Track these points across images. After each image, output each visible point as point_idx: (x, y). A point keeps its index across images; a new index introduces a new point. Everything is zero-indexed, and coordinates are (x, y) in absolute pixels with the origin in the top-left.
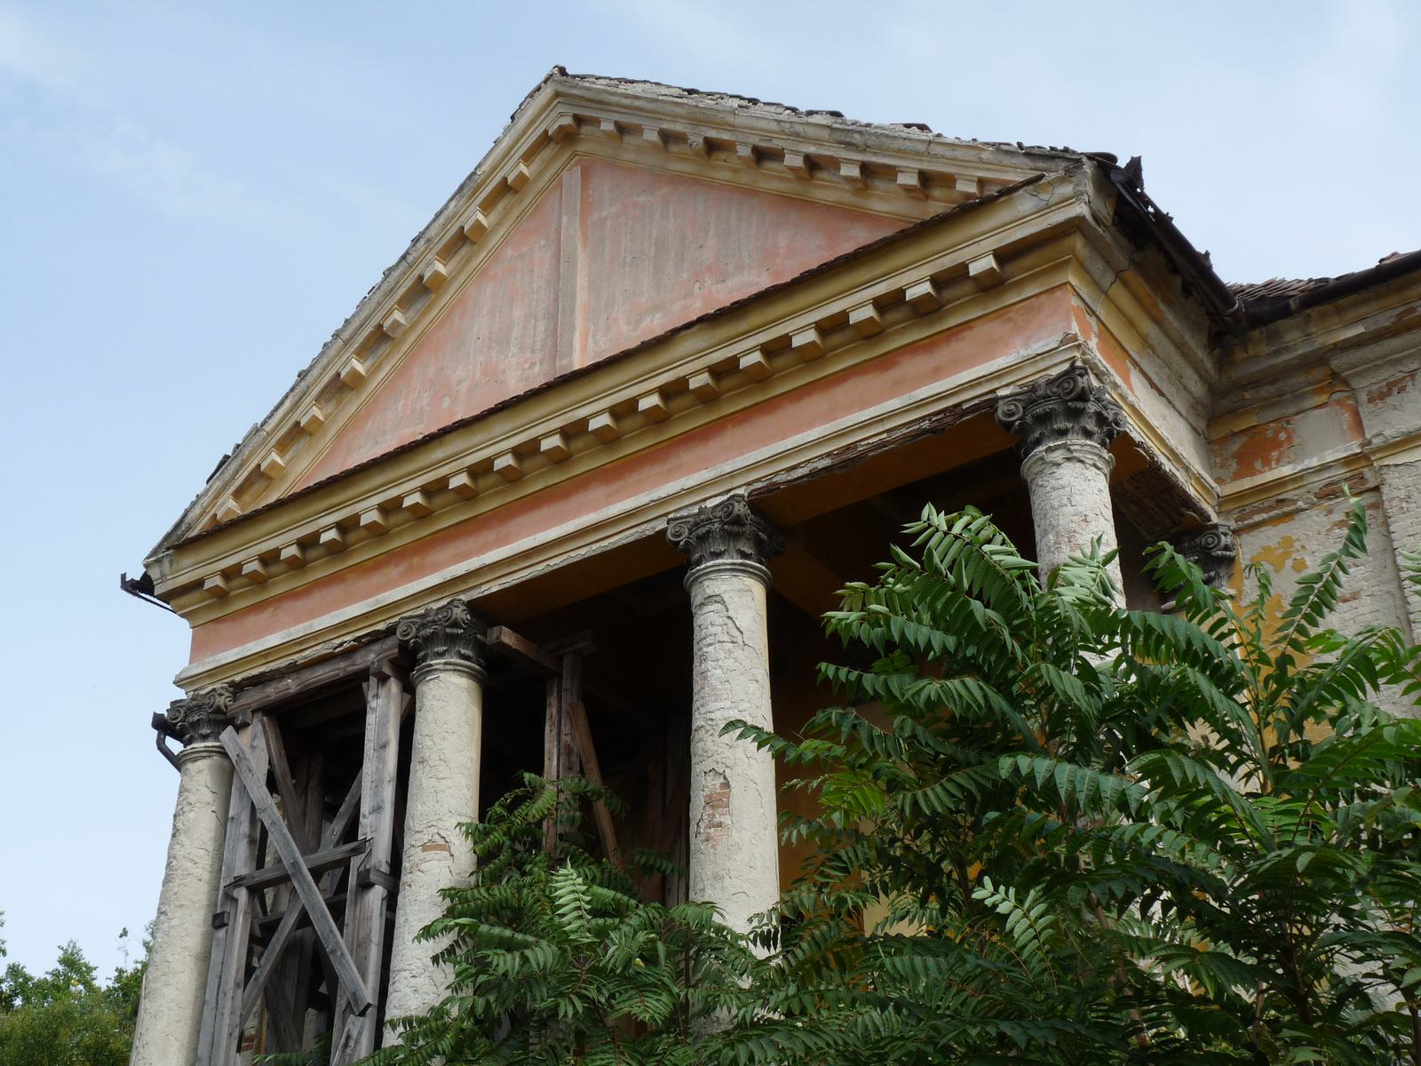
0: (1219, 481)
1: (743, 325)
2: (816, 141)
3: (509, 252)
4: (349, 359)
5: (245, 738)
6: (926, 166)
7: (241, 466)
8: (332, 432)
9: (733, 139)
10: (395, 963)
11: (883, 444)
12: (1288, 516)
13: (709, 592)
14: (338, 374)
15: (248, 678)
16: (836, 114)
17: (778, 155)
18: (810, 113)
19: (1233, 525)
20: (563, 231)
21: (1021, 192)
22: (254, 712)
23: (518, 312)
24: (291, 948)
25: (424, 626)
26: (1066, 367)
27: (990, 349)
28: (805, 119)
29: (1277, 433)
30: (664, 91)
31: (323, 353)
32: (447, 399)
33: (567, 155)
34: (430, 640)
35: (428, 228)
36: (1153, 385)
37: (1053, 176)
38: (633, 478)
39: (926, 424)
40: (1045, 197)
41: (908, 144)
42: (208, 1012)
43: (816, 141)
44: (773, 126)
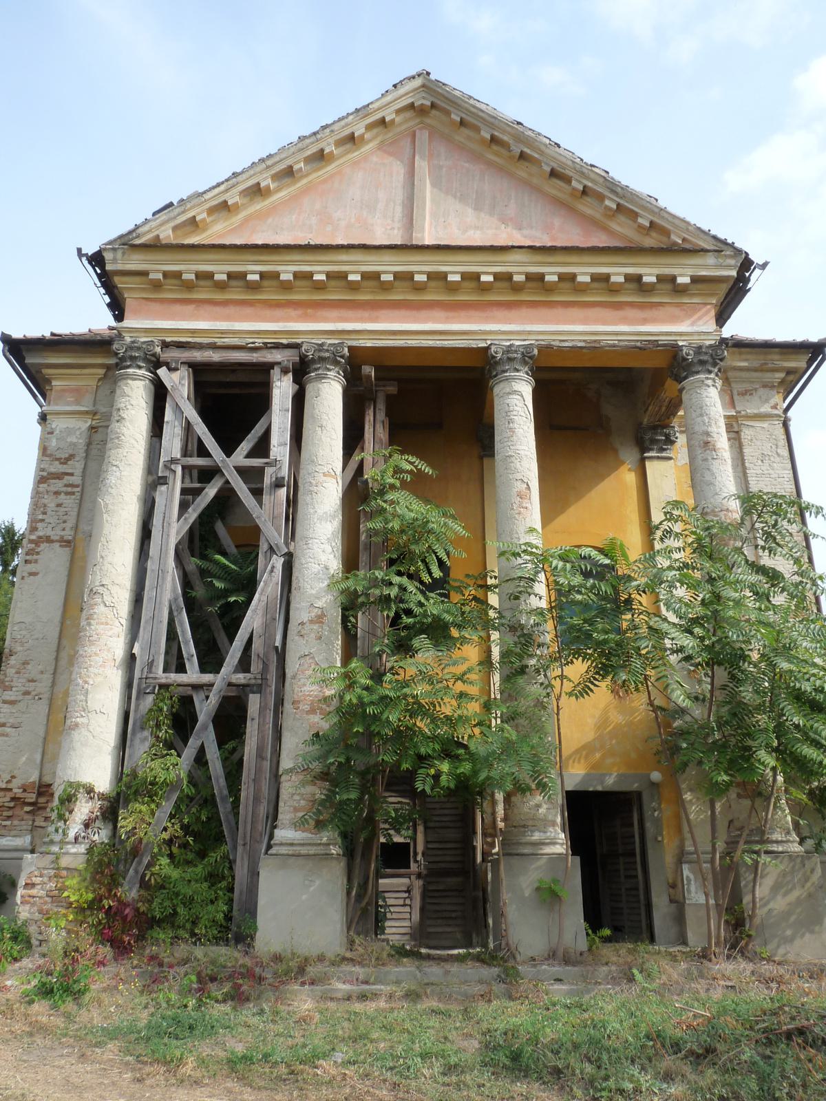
2: (593, 181)
5: (176, 376)
6: (655, 219)
7: (183, 212)
8: (242, 215)
9: (541, 158)
11: (614, 346)
15: (176, 342)
16: (607, 172)
21: (711, 253)
25: (320, 351)
27: (673, 319)
33: (418, 121)
37: (728, 253)
38: (463, 314)
39: (638, 344)
40: (720, 260)
41: (648, 205)
43: (593, 181)
44: (570, 163)
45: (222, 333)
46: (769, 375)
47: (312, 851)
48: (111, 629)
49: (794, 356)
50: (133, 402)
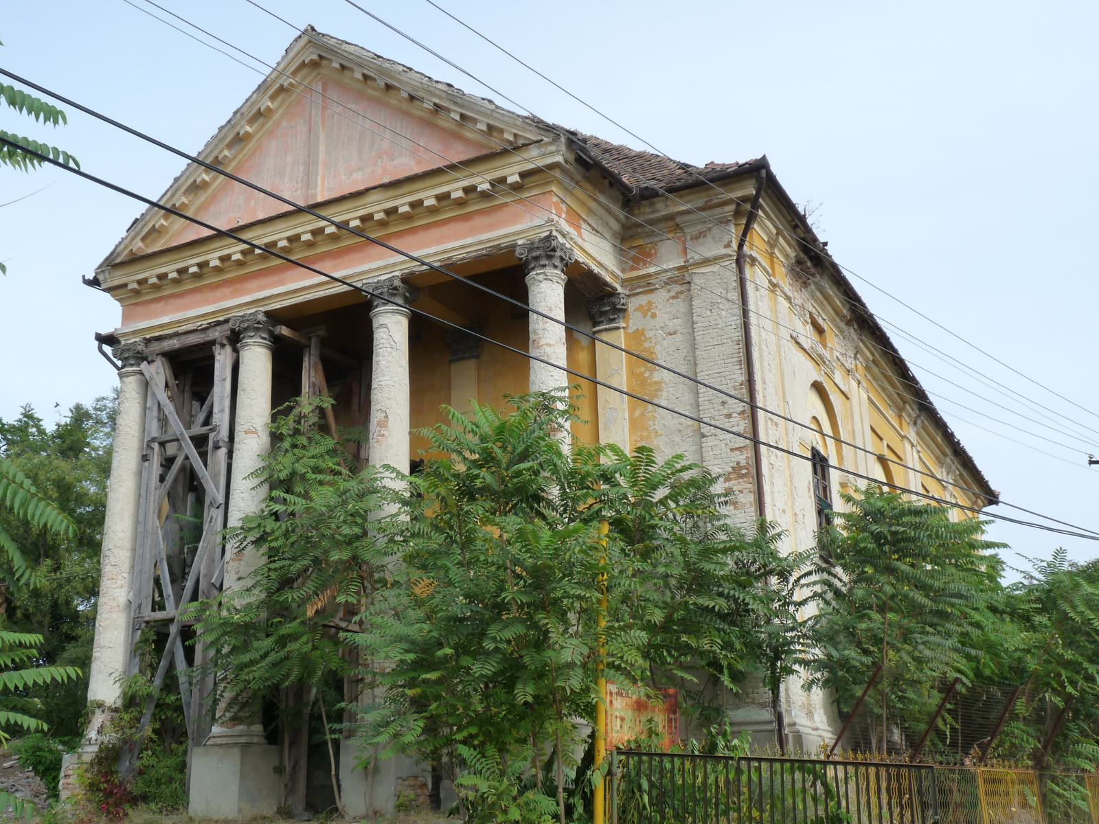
0: (623, 271)
1: (401, 191)
3: (284, 124)
4: (201, 174)
5: (153, 367)
6: (491, 122)
7: (145, 225)
10: (233, 486)
11: (464, 259)
12: (652, 291)
13: (381, 323)
14: (195, 181)
17: (421, 100)
18: (437, 82)
19: (628, 293)
20: (313, 118)
22: (157, 355)
23: (289, 159)
24: (182, 468)
25: (243, 321)
26: (548, 233)
28: (435, 85)
29: (650, 250)
30: (366, 53)
31: (187, 169)
32: (253, 201)
33: (315, 73)
34: (246, 329)
35: (242, 107)
36: (593, 229)
38: (346, 258)
42: (143, 501)
43: (440, 97)
44: (419, 85)
45: (180, 322)
46: (718, 210)
47: (225, 741)
48: (116, 583)
49: (737, 185)
50: (127, 396)
